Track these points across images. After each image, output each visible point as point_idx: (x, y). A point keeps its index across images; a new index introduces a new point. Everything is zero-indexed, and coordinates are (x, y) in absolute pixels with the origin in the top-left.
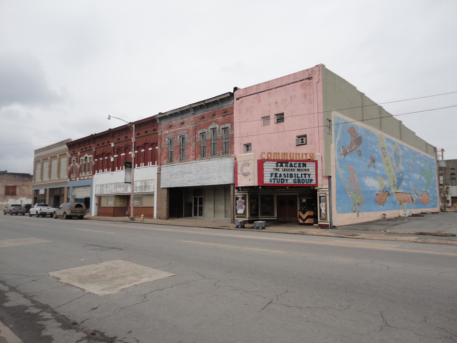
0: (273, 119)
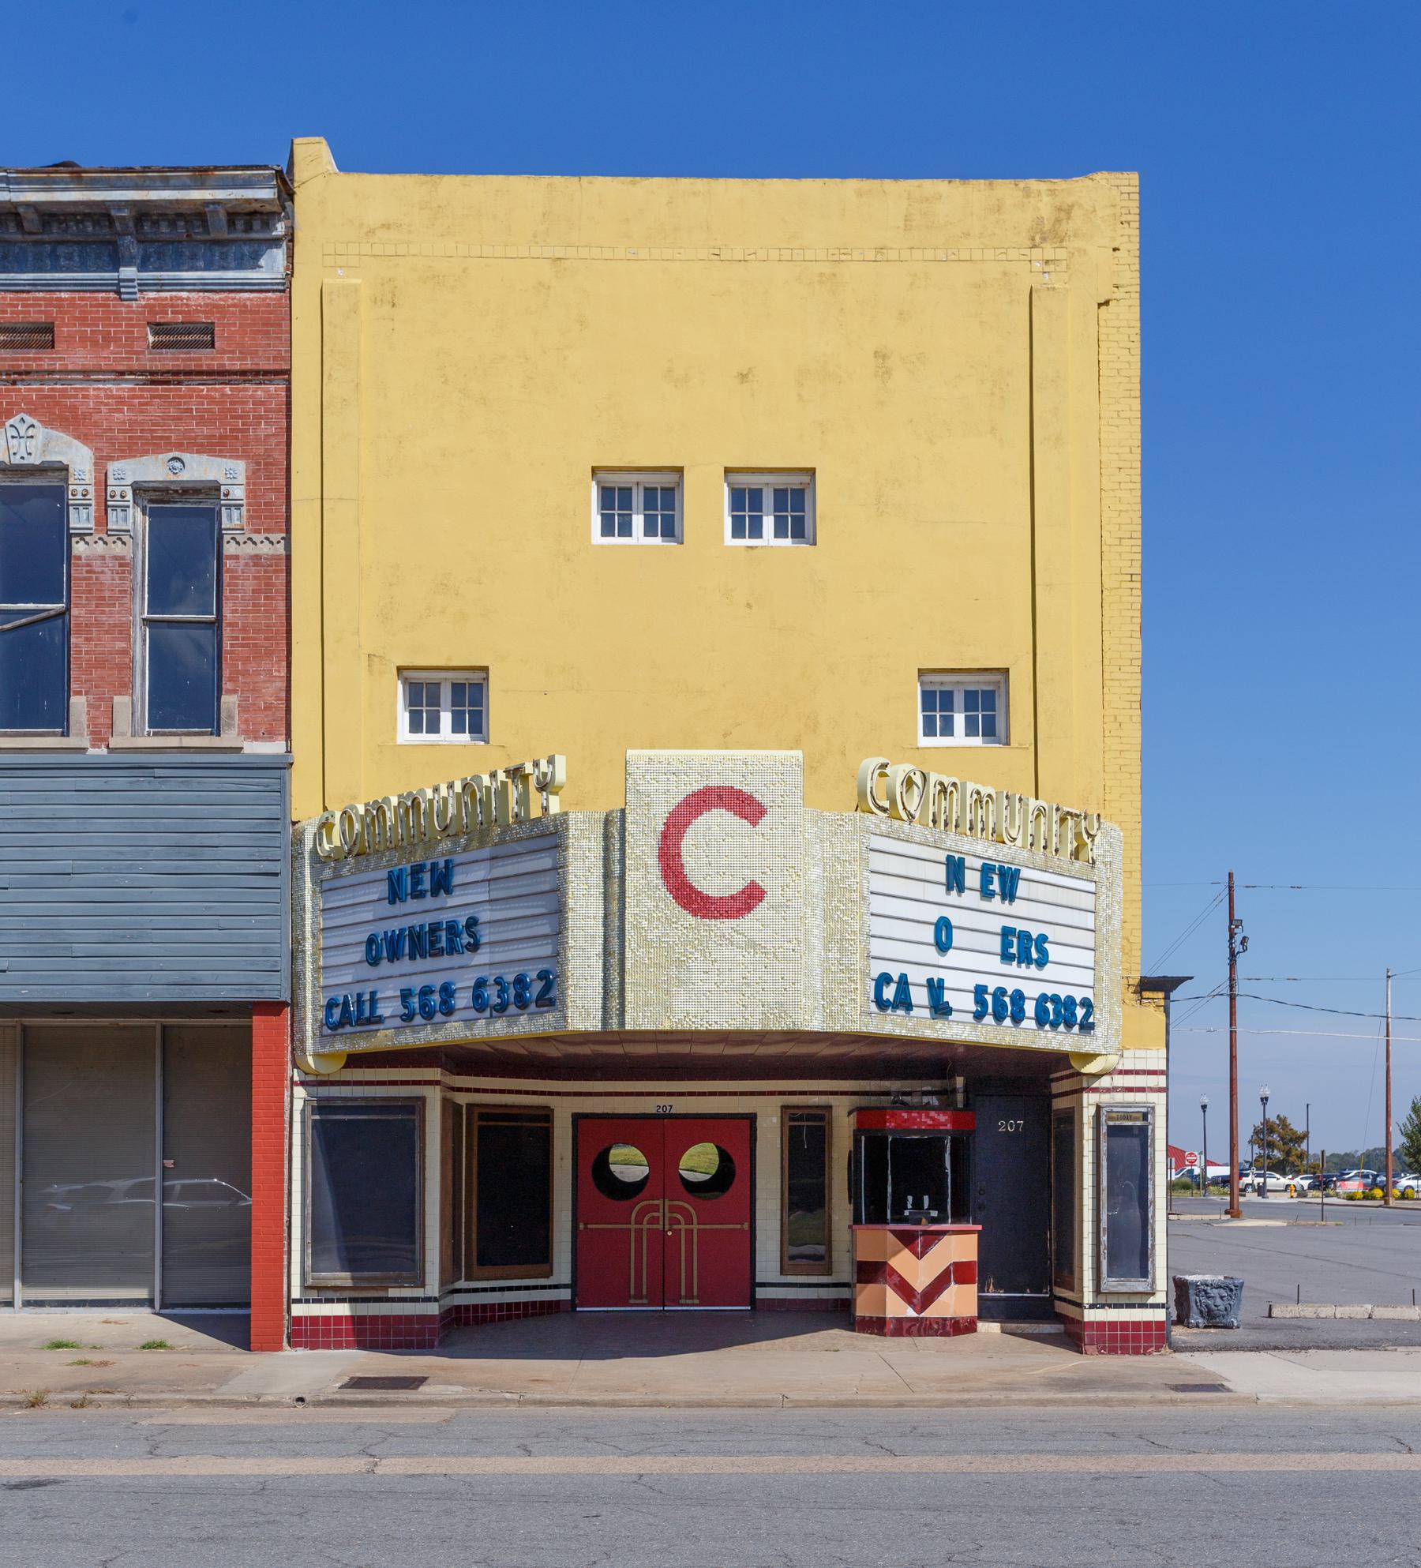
0: (706, 504)
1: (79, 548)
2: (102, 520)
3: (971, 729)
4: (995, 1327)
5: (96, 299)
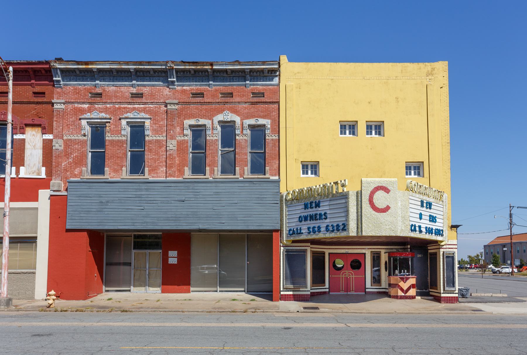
0: (362, 128)
1: (237, 137)
2: (242, 132)
3: (415, 174)
4: (419, 298)
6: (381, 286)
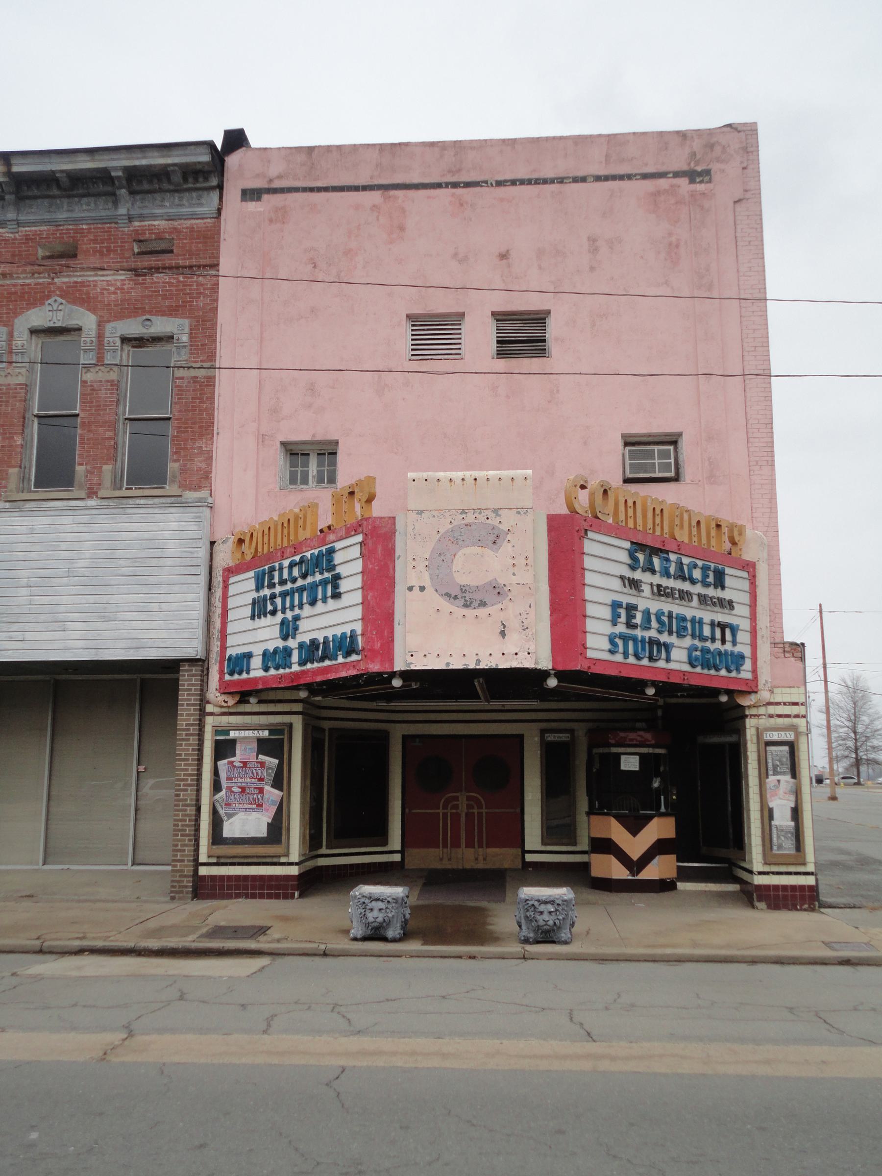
0: (479, 337)
5: (103, 228)
6: (575, 844)
